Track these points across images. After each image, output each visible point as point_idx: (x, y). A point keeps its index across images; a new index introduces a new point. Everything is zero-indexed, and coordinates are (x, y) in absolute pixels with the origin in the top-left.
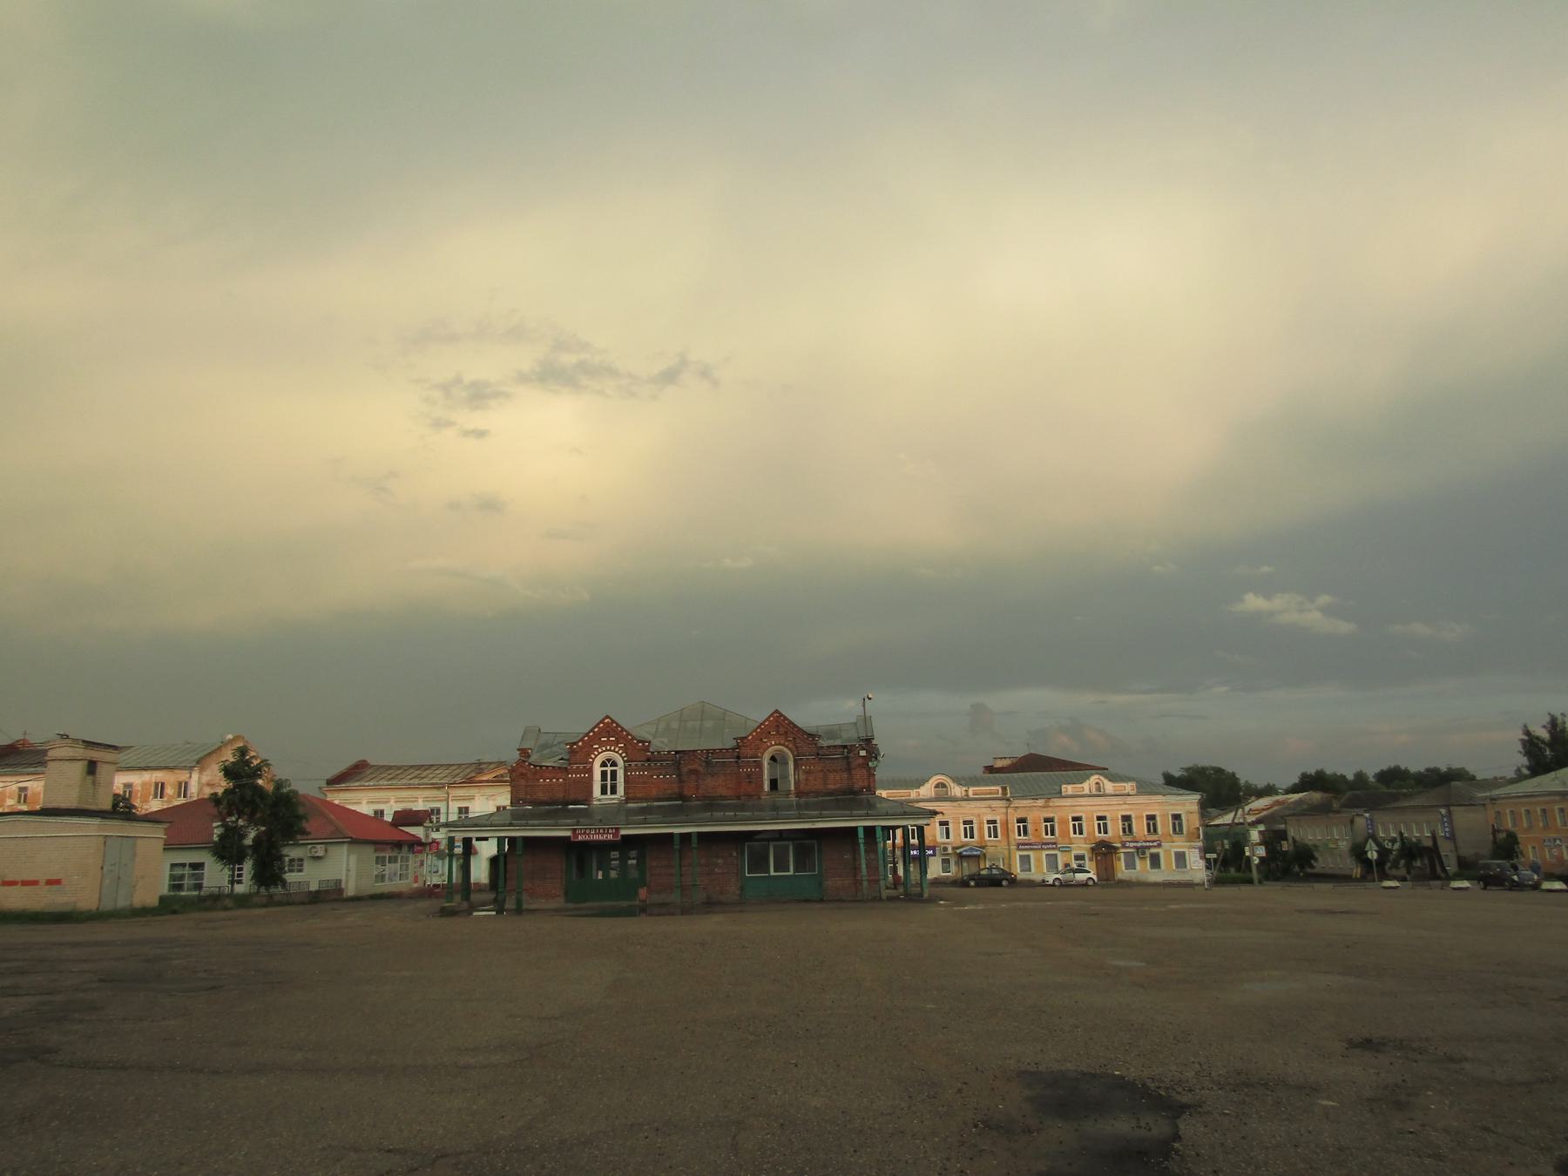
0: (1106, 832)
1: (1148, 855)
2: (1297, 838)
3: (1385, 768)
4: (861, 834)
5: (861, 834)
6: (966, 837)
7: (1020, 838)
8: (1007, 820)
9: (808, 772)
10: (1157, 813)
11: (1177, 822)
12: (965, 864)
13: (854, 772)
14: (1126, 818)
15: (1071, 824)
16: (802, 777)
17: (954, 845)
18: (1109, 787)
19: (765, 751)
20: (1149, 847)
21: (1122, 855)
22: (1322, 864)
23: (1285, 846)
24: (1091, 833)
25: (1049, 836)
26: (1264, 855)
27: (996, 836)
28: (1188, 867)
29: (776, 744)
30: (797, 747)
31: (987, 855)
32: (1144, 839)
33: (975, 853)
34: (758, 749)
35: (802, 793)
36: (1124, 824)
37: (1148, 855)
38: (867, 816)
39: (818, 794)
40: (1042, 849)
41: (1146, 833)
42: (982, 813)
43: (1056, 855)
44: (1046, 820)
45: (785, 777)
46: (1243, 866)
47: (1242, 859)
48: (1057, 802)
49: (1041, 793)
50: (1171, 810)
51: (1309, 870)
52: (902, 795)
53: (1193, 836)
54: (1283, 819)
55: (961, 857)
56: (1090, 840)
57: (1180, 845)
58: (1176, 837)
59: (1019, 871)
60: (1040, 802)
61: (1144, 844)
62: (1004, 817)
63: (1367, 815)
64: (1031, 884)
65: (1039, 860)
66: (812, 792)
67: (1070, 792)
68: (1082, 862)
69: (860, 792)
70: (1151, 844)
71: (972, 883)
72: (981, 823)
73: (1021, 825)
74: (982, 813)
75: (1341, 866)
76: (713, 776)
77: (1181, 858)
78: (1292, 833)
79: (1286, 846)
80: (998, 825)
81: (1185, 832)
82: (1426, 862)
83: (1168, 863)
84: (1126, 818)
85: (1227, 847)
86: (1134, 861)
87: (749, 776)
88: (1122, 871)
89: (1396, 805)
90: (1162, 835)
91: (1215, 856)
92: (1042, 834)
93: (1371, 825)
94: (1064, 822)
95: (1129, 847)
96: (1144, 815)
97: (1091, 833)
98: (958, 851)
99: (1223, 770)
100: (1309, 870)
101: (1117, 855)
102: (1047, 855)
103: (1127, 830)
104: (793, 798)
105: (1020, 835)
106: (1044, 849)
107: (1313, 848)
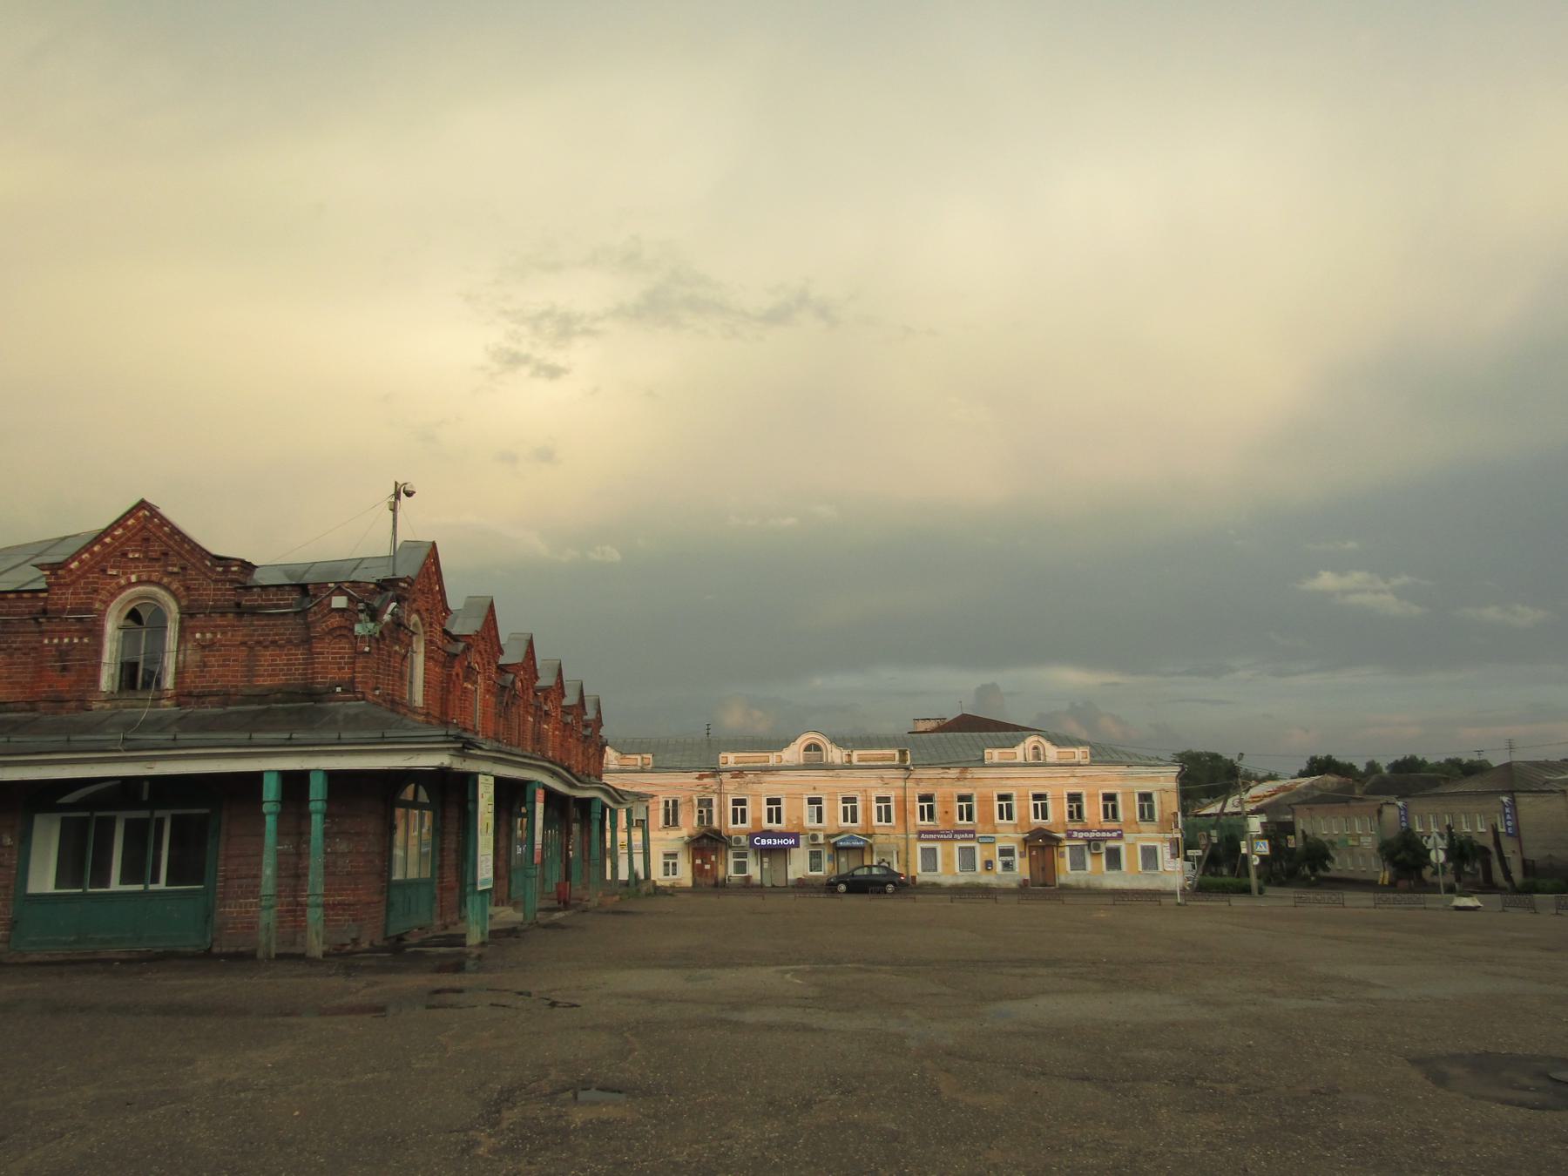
0: (1045, 817)
1: (1103, 849)
3: (1400, 758)
4: (271, 790)
6: (845, 820)
8: (905, 797)
9: (203, 647)
12: (843, 860)
13: (318, 646)
14: (1075, 798)
15: (997, 804)
16: (193, 657)
17: (829, 832)
18: (1052, 753)
19: (113, 596)
20: (1105, 839)
21: (1067, 850)
22: (1340, 865)
23: (1292, 842)
24: (1023, 818)
25: (965, 821)
26: (1267, 853)
27: (888, 820)
28: (1161, 869)
29: (139, 582)
30: (188, 589)
32: (1098, 827)
33: (856, 843)
34: (96, 591)
35: (190, 694)
36: (1071, 806)
37: (1103, 849)
39: (226, 697)
40: (954, 839)
42: (869, 786)
43: (973, 848)
44: (961, 798)
45: (156, 657)
46: (1238, 865)
48: (978, 773)
49: (957, 760)
51: (1322, 873)
52: (757, 759)
53: (1165, 826)
55: (837, 849)
57: (1149, 835)
58: (1144, 826)
59: (919, 870)
60: (954, 773)
61: (1098, 835)
62: (901, 793)
63: (1400, 804)
64: (935, 888)
65: (949, 855)
66: (211, 694)
67: (996, 759)
68: (1009, 858)
69: (327, 694)
70: (1109, 835)
71: (842, 887)
72: (867, 801)
73: (925, 805)
74: (869, 786)
75: (1364, 869)
77: (1150, 855)
78: (1300, 825)
80: (892, 805)
81: (1157, 817)
82: (1478, 865)
83: (1133, 863)
84: (1075, 798)
87: (63, 653)
88: (1066, 872)
89: (1440, 790)
91: (1199, 853)
92: (953, 818)
93: (1406, 817)
94: (985, 801)
95: (1077, 839)
96: (1100, 792)
98: (833, 841)
99: (1221, 757)
100: (1322, 873)
101: (1060, 849)
102: (960, 848)
103: (1075, 814)
104: (168, 706)
105: (922, 818)
106: (956, 840)
107: (1328, 845)
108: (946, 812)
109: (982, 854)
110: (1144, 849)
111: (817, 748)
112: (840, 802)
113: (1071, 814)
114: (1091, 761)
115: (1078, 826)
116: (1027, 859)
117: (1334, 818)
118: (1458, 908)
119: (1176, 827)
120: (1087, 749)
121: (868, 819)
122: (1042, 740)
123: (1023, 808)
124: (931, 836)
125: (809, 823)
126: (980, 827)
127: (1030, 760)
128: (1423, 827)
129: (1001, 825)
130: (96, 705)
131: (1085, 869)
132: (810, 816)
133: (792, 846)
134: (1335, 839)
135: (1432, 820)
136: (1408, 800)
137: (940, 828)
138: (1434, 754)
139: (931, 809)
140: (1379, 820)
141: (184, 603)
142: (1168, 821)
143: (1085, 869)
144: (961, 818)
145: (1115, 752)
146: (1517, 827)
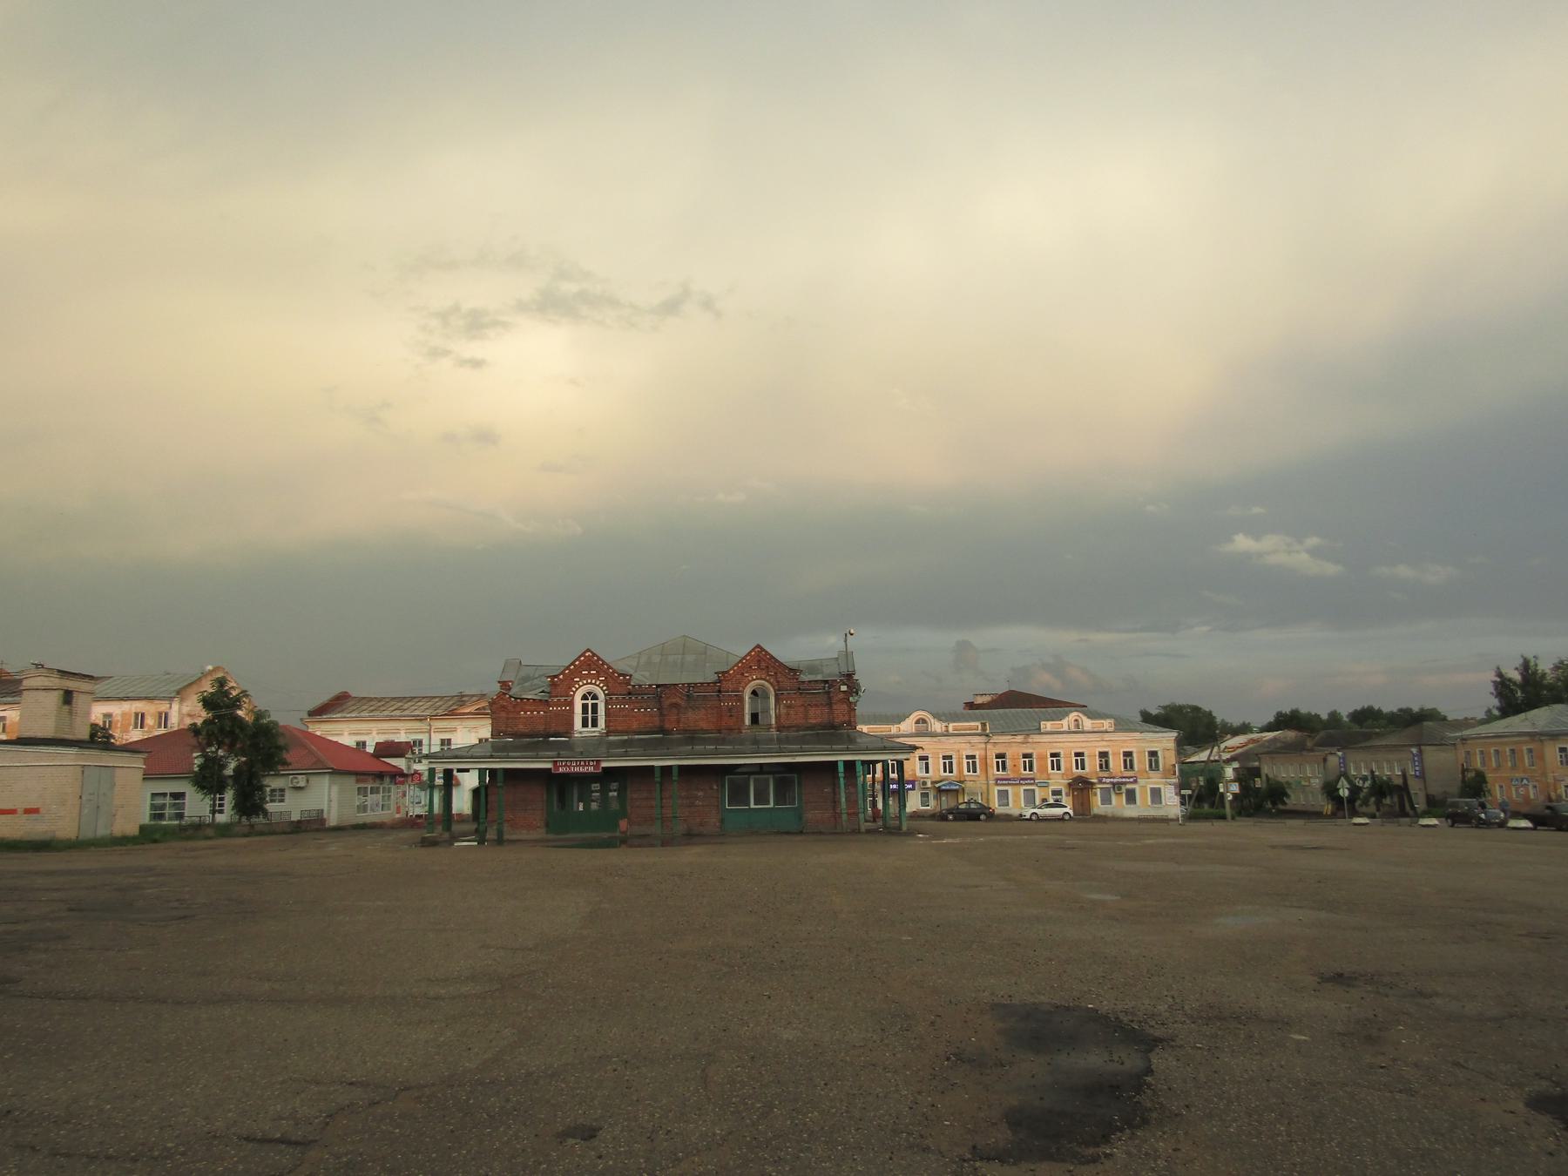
0: (1083, 768)
1: (1124, 790)
2: (1271, 776)
4: (841, 768)
5: (841, 768)
6: (945, 771)
9: (789, 707)
11: (1153, 759)
12: (944, 798)
13: (835, 707)
14: (1104, 755)
15: (1050, 759)
16: (783, 711)
18: (1088, 724)
20: (1125, 783)
21: (1098, 791)
22: (1295, 800)
23: (1258, 783)
25: (1027, 772)
27: (975, 771)
29: (757, 679)
30: (778, 682)
31: (966, 791)
32: (1120, 775)
35: (784, 727)
37: (1124, 790)
39: (798, 728)
42: (960, 748)
43: (1033, 790)
44: (1025, 756)
45: (767, 711)
48: (1037, 738)
49: (1020, 729)
51: (1281, 807)
52: (875, 730)
53: (1169, 773)
54: (1257, 756)
55: (939, 791)
57: (1155, 780)
58: (1152, 773)
59: (997, 806)
60: (1019, 738)
61: (1120, 780)
63: (1340, 754)
64: (1008, 818)
65: (1016, 795)
67: (1049, 729)
68: (1058, 797)
70: (1128, 780)
72: (960, 759)
73: (1000, 760)
74: (960, 748)
77: (1156, 794)
78: (1265, 770)
80: (977, 761)
82: (1396, 799)
84: (1104, 755)
85: (1202, 783)
90: (1138, 771)
91: (1189, 792)
94: (1042, 758)
95: (1105, 783)
98: (937, 785)
99: (1200, 709)
100: (1281, 807)
102: (1025, 790)
104: (774, 732)
105: (998, 770)
107: (1286, 786)
108: (1015, 766)
109: (1040, 795)
110: (1152, 789)
111: (924, 721)
112: (941, 759)
113: (1101, 766)
114: (1115, 729)
115: (1106, 774)
116: (1071, 797)
117: (1292, 764)
118: (1355, 824)
119: (1175, 774)
120: (1112, 721)
121: (960, 771)
122: (1080, 715)
123: (1067, 762)
124: (1004, 782)
125: (920, 773)
126: (1038, 775)
127: (1073, 729)
128: (1390, 771)
129: (1054, 774)
130: (744, 731)
131: (1111, 804)
132: (920, 769)
133: (910, 789)
134: (1291, 781)
135: (1362, 765)
136: (1345, 751)
137: (1011, 776)
138: (1389, 705)
139: (1004, 763)
140: (1324, 768)
141: (776, 688)
142: (1169, 770)
143: (1111, 804)
144: (1025, 770)
145: (1131, 722)
146: (1423, 771)
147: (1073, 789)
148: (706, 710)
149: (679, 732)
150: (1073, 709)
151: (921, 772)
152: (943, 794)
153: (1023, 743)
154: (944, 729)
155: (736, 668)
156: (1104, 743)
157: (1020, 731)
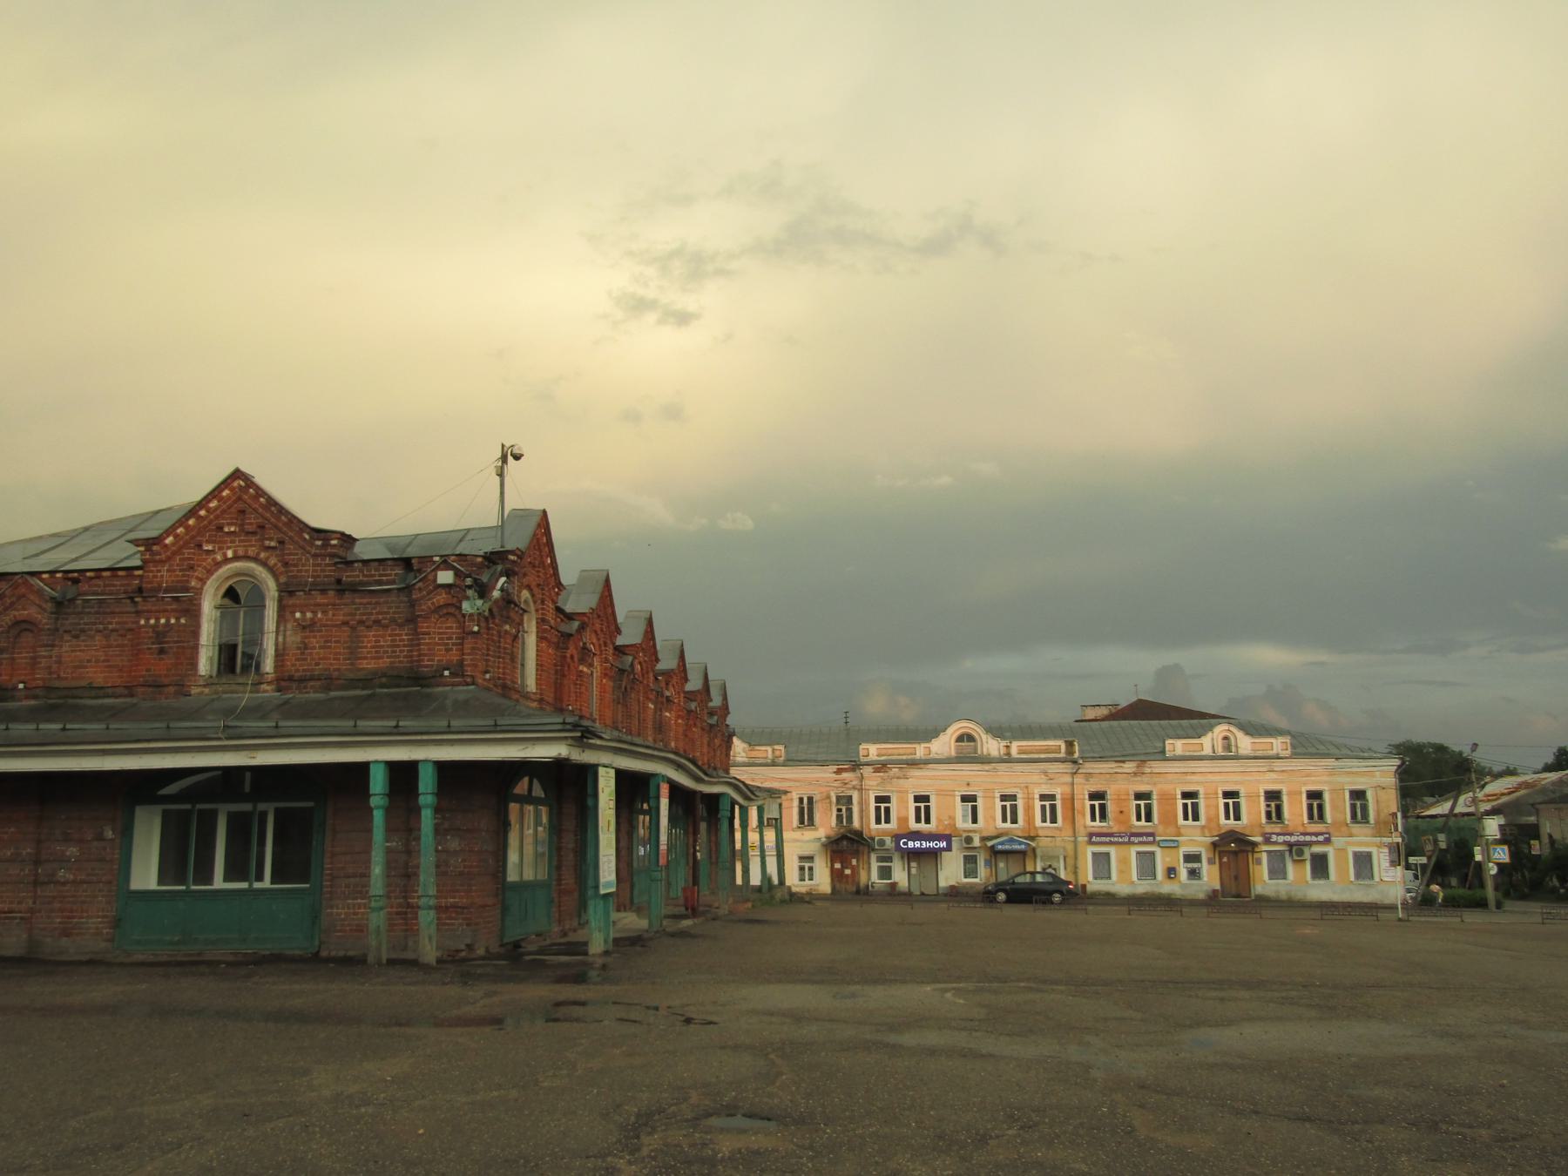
0: (1237, 818)
1: (1307, 855)
2: (1557, 836)
4: (378, 782)
5: (378, 782)
7: (1093, 824)
8: (1073, 794)
10: (1326, 789)
11: (1358, 803)
12: (1001, 865)
13: (424, 626)
14: (1273, 796)
15: (1180, 802)
16: (293, 638)
17: (985, 834)
18: (1245, 743)
19: (210, 572)
20: (1310, 844)
21: (1264, 857)
23: (1536, 848)
24: (1213, 819)
25: (1143, 823)
27: (1054, 821)
28: (1377, 878)
29: (236, 558)
30: (286, 564)
31: (1039, 852)
32: (1301, 830)
34: (191, 568)
35: (291, 679)
36: (1268, 806)
37: (1307, 855)
38: (397, 735)
39: (328, 682)
40: (1130, 843)
41: (1306, 820)
42: (1031, 783)
43: (1153, 853)
44: (1139, 796)
45: (255, 639)
47: (1469, 865)
48: (1158, 766)
49: (1133, 752)
50: (1350, 783)
52: (901, 751)
53: (1382, 828)
54: (1535, 808)
55: (995, 853)
56: (1210, 830)
57: (1362, 840)
58: (1356, 828)
59: (1090, 878)
60: (1129, 767)
61: (1302, 838)
62: (1068, 789)
64: (1109, 898)
65: (1124, 861)
67: (1179, 751)
68: (1195, 865)
69: (434, 678)
70: (1314, 839)
72: (1029, 799)
73: (1096, 803)
76: (76, 637)
77: (1363, 862)
78: (1547, 828)
79: (1538, 847)
80: (1058, 803)
83: (1342, 871)
84: (1273, 796)
85: (1443, 845)
86: (1285, 865)
87: (160, 635)
90: (1334, 823)
91: (1424, 860)
94: (1167, 799)
95: (1276, 843)
97: (1213, 819)
98: (990, 844)
101: (1256, 855)
102: (1138, 853)
103: (1274, 815)
104: (268, 692)
106: (1133, 843)
108: (1121, 812)
109: (1163, 860)
110: (1357, 856)
111: (971, 738)
113: (1269, 815)
119: (1396, 830)
120: (1288, 740)
124: (1103, 839)
126: (1160, 829)
127: (1220, 751)
130: (194, 691)
131: (1285, 878)
137: (1115, 830)
142: (1386, 823)
143: (1285, 878)
144: (1139, 819)
145: (1321, 742)
147: (1220, 852)
148: (107, 637)
149: (30, 692)
150: (1220, 720)
151: (965, 821)
152: (999, 856)
153: (1135, 774)
154: (1003, 751)
155: (180, 530)
156: (1273, 776)
157: (1133, 755)
